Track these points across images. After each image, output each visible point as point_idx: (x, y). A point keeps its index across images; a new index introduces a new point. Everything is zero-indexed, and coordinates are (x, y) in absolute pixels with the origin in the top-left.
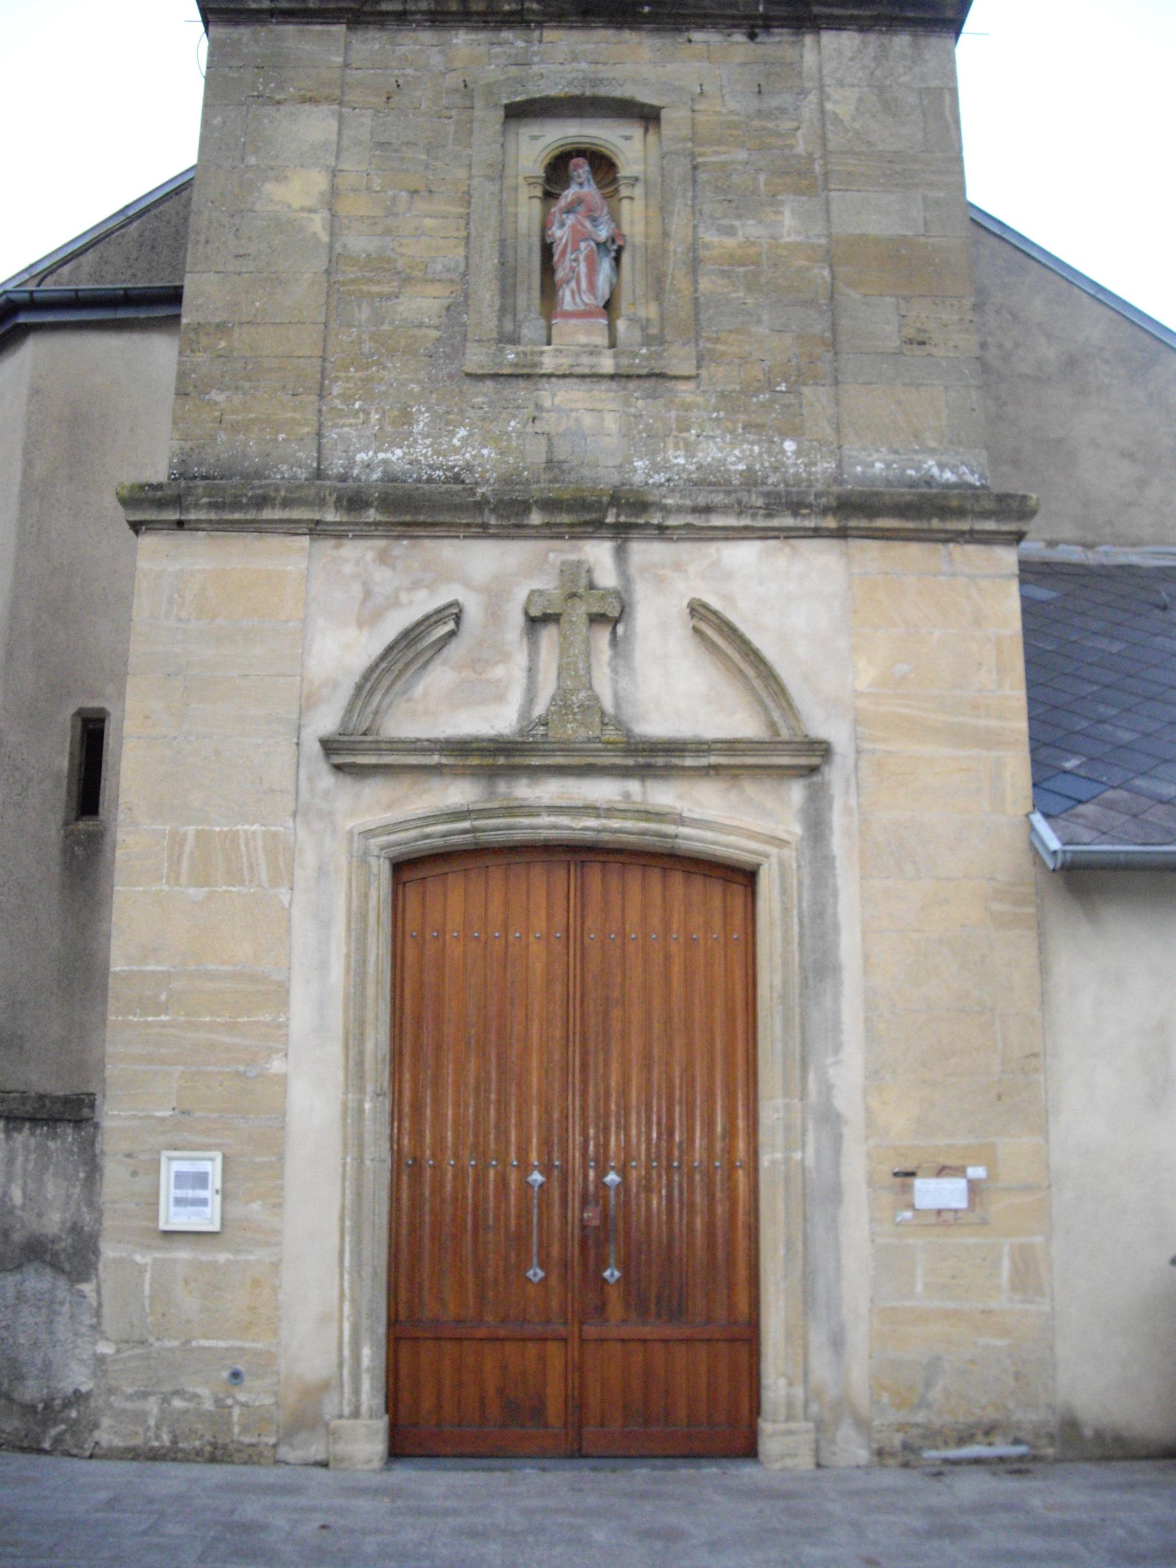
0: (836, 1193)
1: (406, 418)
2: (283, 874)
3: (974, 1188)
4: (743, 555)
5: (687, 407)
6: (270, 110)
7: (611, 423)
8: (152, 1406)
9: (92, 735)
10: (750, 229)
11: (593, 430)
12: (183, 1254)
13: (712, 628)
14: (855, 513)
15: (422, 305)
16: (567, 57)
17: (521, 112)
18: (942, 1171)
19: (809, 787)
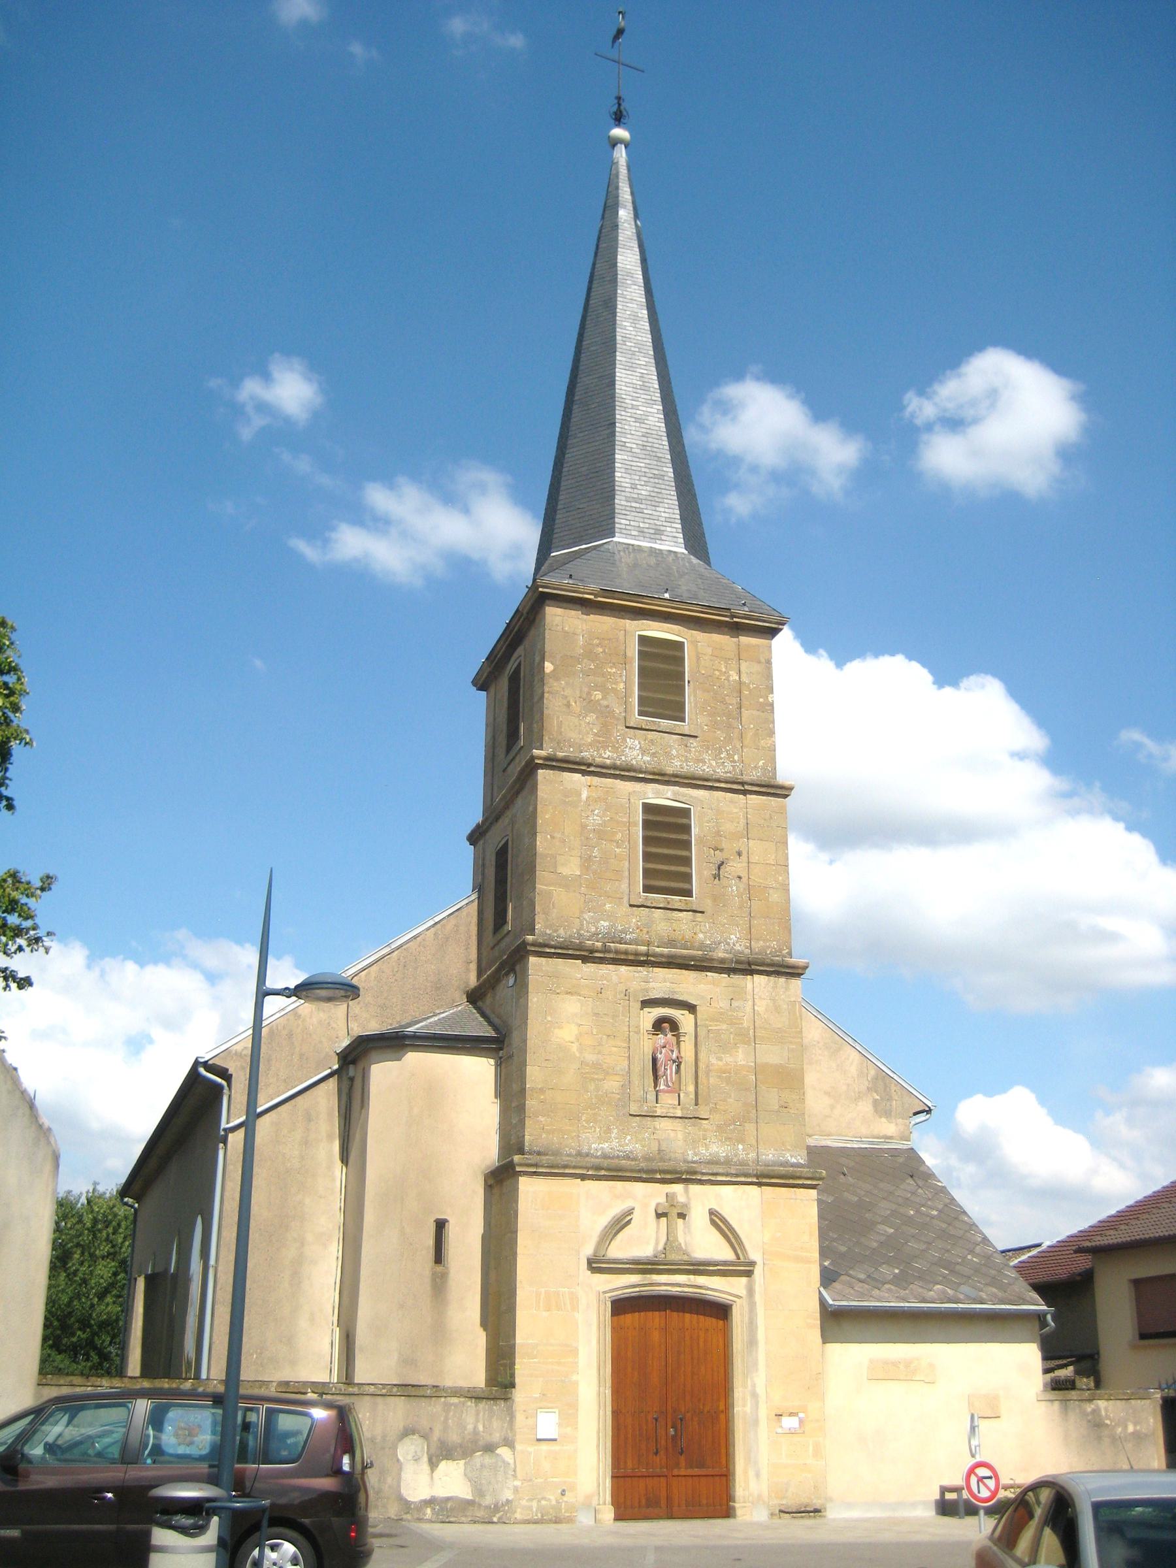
0: (756, 1422)
1: (609, 1130)
2: (575, 1308)
3: (801, 1422)
5: (705, 1130)
6: (554, 996)
7: (680, 1136)
8: (534, 1504)
9: (441, 1225)
10: (728, 1059)
11: (675, 1139)
12: (544, 1447)
13: (717, 1220)
14: (765, 1178)
15: (612, 1085)
17: (647, 1003)
18: (791, 1414)
19: (498, 1065)
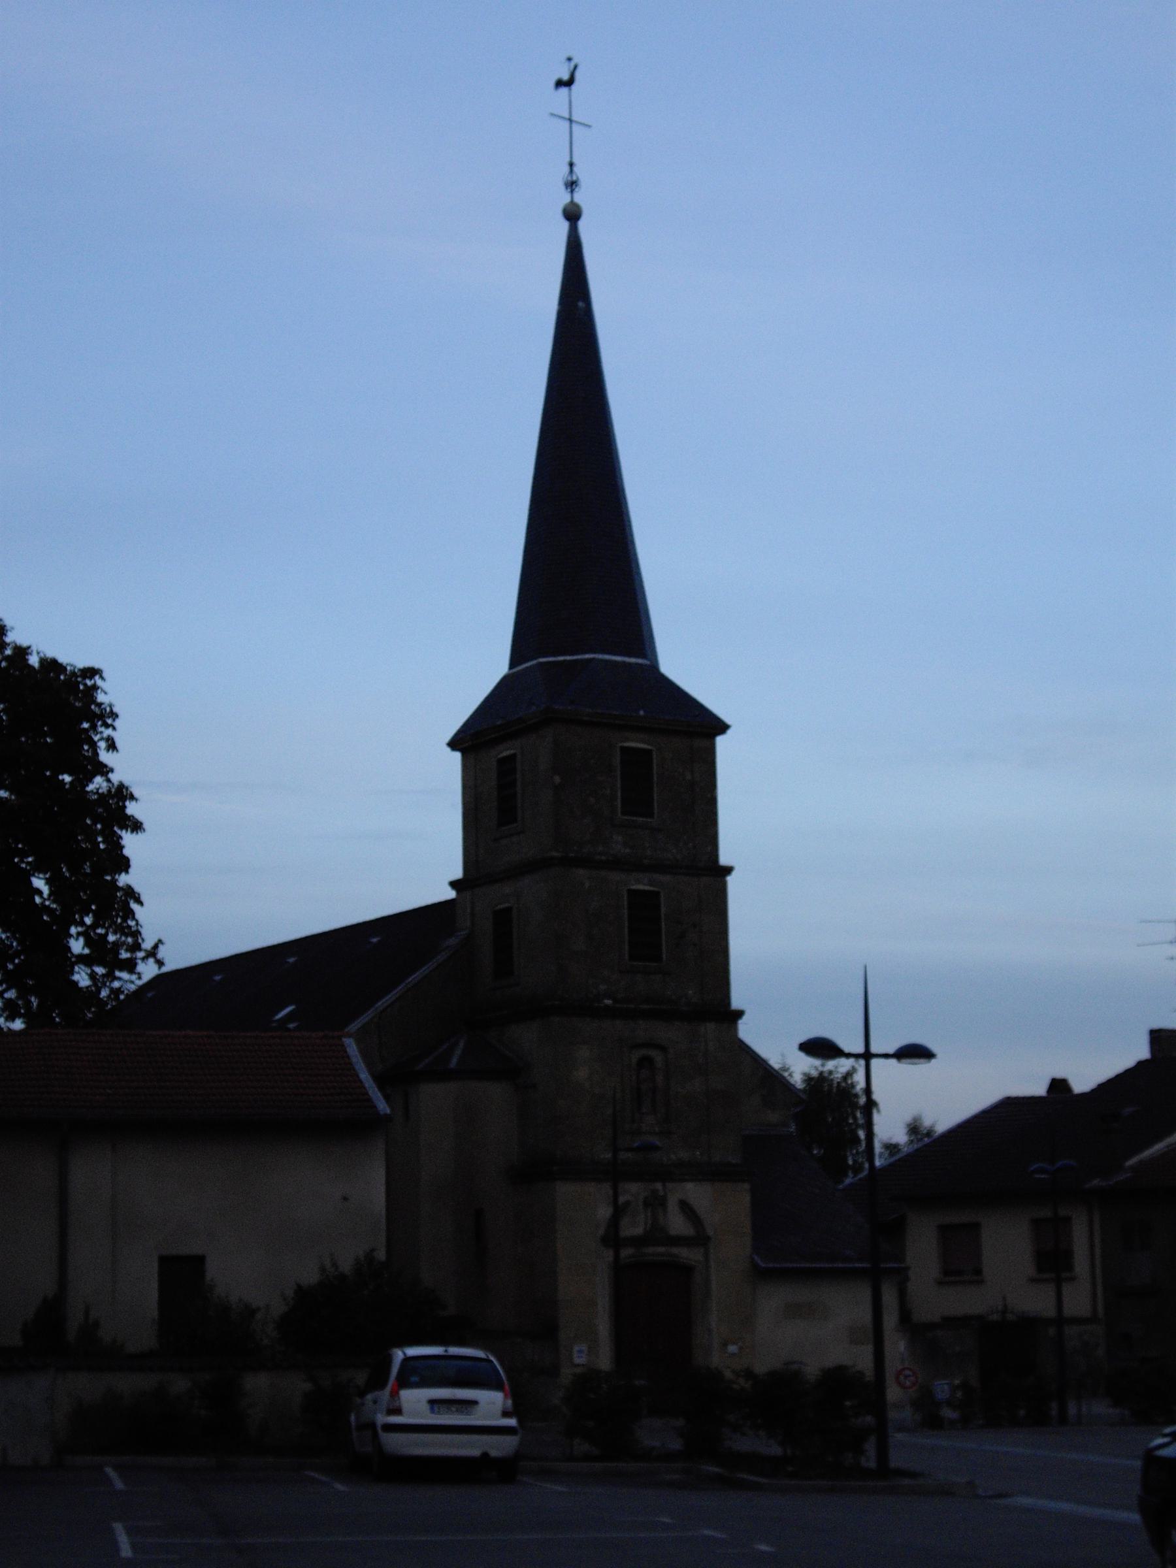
4: (690, 1186)
16: (897, 1157)
